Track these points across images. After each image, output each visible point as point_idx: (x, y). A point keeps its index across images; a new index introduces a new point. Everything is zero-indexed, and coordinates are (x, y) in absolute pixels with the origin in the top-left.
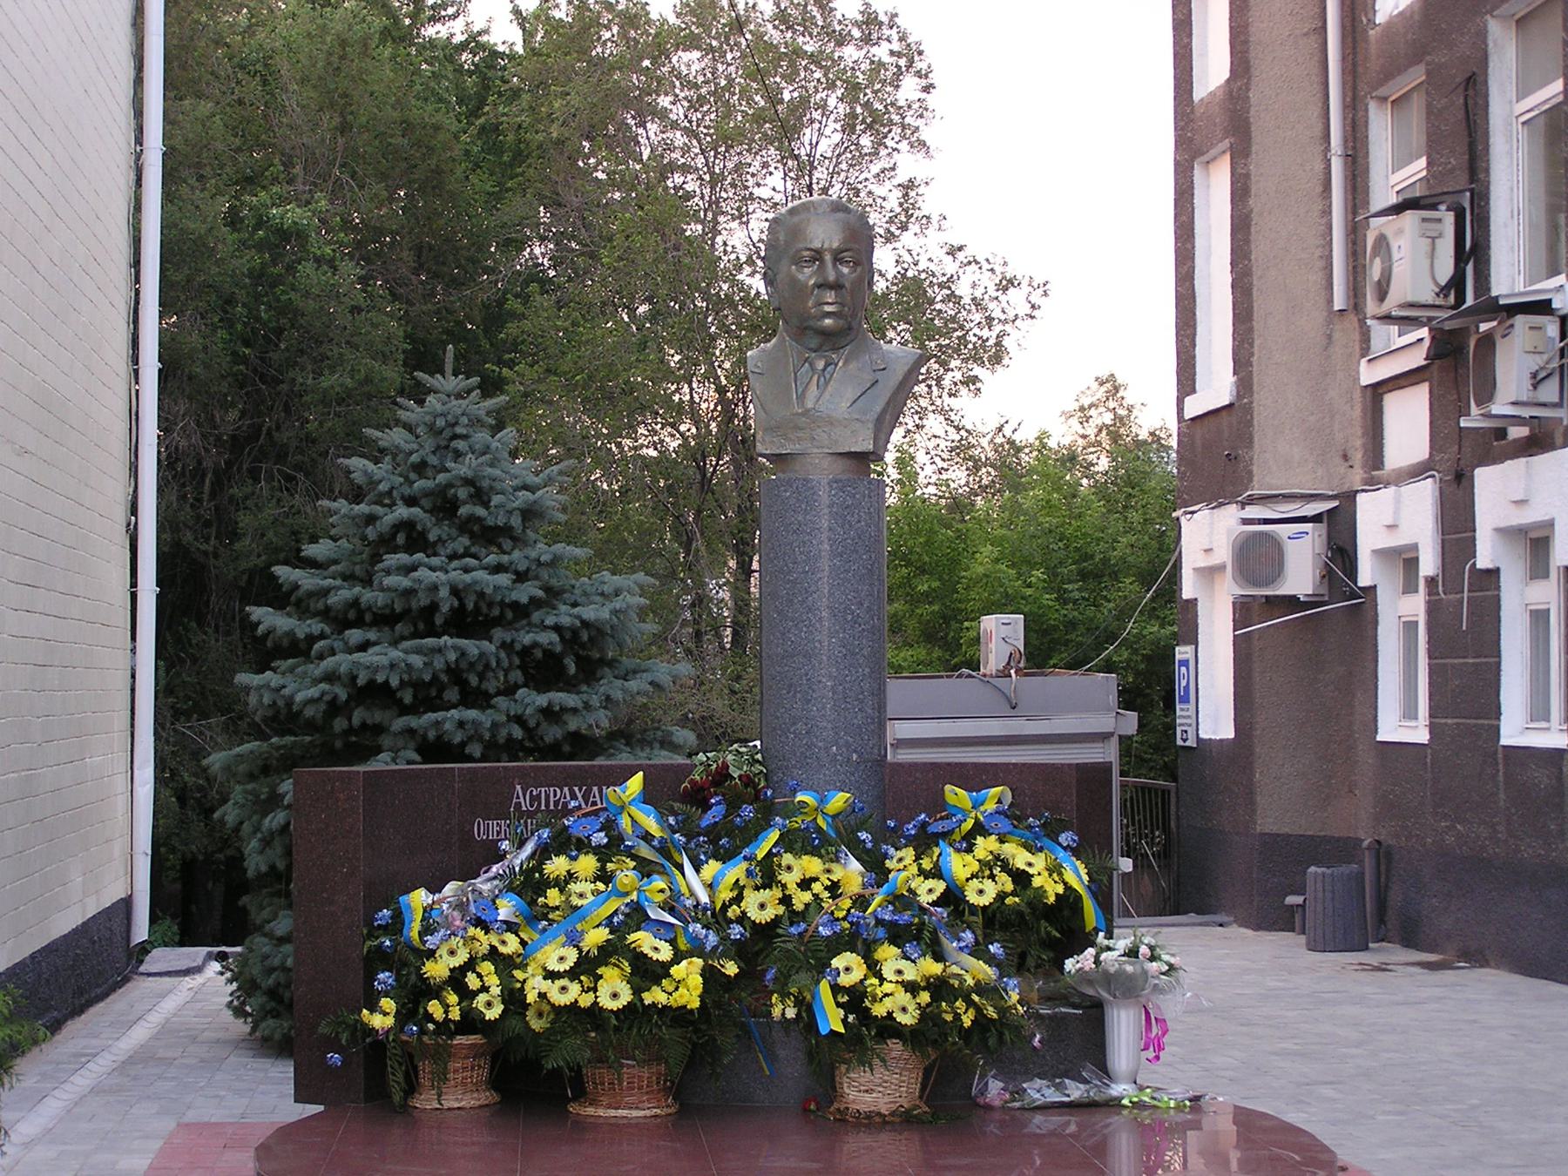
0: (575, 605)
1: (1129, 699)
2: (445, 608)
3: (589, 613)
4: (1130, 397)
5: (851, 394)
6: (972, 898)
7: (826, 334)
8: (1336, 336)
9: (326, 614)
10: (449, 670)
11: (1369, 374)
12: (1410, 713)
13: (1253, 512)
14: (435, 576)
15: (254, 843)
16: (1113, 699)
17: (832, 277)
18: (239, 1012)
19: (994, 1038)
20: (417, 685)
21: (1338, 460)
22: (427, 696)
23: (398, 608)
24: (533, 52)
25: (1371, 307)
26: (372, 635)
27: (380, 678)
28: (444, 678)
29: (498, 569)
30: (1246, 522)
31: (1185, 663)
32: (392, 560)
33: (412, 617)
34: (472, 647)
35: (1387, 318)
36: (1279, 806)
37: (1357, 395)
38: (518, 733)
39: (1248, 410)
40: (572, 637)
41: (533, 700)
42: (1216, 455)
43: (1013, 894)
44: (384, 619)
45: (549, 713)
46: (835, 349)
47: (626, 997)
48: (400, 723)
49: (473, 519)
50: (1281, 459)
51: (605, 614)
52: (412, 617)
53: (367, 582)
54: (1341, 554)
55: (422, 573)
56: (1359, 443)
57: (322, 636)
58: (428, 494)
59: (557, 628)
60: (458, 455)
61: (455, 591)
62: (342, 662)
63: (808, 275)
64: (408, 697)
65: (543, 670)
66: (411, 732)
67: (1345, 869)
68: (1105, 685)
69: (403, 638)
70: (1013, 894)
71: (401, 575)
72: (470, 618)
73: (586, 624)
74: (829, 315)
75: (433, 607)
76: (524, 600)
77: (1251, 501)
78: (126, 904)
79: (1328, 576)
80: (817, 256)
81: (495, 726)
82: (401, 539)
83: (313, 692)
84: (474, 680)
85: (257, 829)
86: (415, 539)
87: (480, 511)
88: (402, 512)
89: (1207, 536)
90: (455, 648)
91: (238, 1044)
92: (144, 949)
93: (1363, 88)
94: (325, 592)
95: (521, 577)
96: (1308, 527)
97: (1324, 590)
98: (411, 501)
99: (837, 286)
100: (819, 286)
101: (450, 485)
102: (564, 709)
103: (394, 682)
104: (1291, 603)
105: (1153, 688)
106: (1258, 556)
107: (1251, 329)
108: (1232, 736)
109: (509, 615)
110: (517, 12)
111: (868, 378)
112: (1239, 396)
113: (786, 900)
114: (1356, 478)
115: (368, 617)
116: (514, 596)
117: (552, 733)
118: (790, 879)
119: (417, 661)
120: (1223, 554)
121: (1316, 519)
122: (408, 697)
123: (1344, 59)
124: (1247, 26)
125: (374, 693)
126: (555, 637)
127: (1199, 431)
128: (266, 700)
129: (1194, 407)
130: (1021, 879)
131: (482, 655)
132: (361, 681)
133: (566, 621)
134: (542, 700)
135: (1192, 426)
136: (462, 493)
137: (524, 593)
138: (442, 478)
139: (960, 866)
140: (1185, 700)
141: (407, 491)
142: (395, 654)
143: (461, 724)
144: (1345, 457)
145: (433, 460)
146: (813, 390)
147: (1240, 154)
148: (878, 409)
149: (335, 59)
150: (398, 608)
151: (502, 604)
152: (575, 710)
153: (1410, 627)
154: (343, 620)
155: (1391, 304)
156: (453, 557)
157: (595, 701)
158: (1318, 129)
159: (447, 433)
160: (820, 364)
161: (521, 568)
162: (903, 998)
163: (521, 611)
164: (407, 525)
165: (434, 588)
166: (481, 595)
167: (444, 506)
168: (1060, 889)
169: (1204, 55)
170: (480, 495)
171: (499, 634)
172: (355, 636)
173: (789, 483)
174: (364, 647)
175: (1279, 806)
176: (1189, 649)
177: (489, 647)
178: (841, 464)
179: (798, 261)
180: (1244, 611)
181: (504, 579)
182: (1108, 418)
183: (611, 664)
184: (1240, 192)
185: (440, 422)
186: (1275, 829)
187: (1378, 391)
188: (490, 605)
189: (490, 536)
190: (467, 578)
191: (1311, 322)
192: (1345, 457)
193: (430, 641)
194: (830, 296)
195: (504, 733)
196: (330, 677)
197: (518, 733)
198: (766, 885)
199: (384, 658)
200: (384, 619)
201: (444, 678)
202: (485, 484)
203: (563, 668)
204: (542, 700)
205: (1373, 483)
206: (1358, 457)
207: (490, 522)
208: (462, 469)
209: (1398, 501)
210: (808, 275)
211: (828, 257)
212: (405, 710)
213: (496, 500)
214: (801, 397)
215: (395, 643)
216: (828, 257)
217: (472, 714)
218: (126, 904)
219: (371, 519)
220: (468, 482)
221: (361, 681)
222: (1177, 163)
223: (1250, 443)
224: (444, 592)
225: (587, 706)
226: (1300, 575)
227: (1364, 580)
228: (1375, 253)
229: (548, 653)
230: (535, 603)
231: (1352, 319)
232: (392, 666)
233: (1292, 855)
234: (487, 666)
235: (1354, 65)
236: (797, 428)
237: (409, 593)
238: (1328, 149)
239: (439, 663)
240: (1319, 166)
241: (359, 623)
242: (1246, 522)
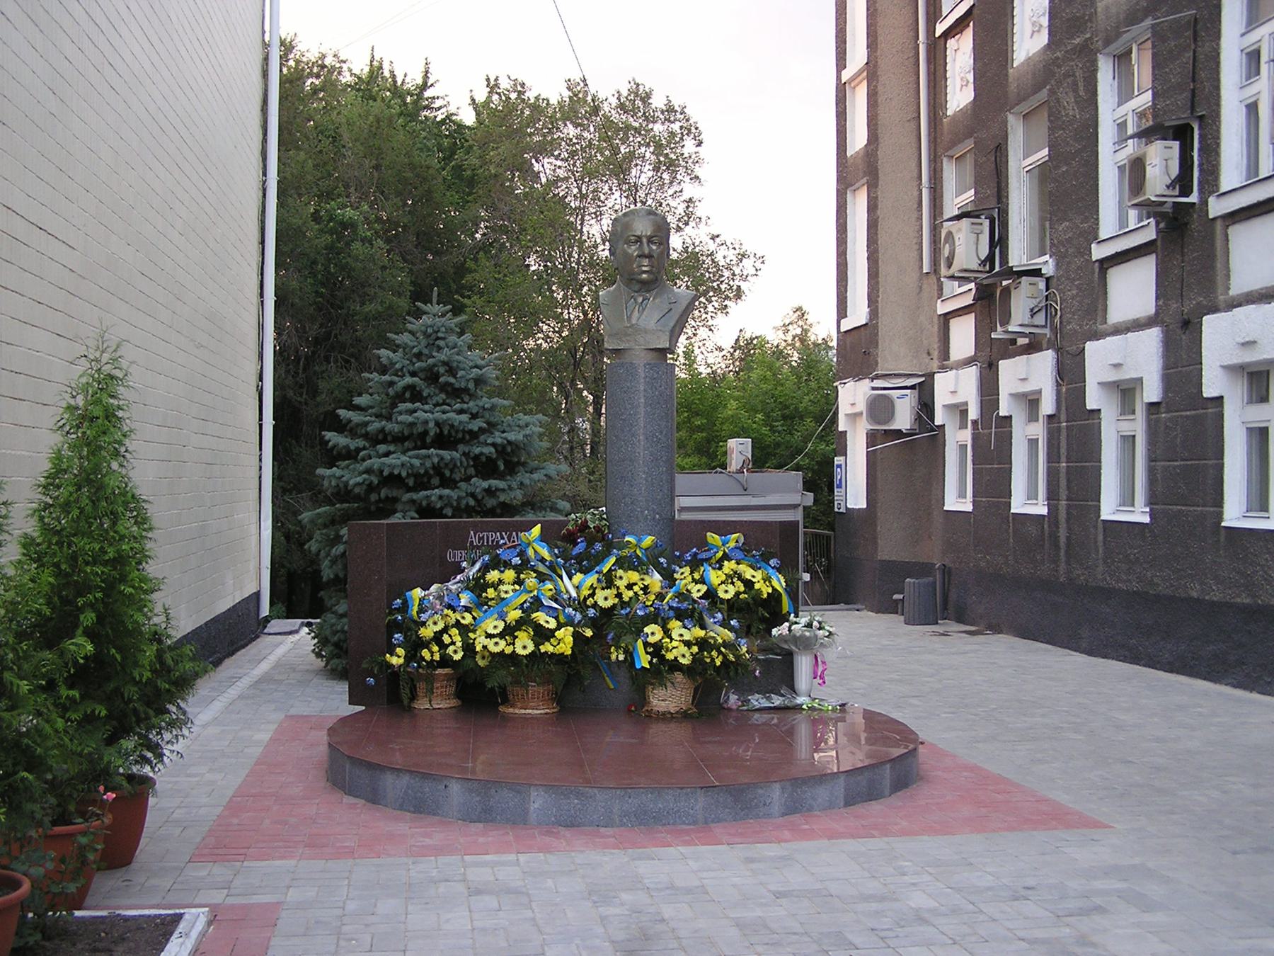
0: (504, 432)
1: (808, 486)
2: (432, 434)
3: (511, 436)
4: (811, 318)
5: (657, 316)
6: (722, 595)
7: (643, 282)
8: (925, 286)
9: (366, 436)
10: (434, 467)
11: (942, 308)
12: (962, 494)
13: (878, 383)
14: (425, 416)
15: (327, 562)
16: (800, 485)
17: (647, 251)
18: (318, 655)
19: (733, 672)
20: (416, 476)
21: (925, 355)
22: (422, 482)
23: (406, 433)
24: (480, 122)
25: (944, 271)
26: (392, 448)
27: (396, 472)
28: (431, 472)
29: (461, 412)
30: (873, 389)
31: (839, 466)
32: (403, 406)
33: (415, 439)
34: (446, 454)
35: (952, 277)
36: (891, 544)
37: (936, 320)
38: (472, 502)
39: (876, 327)
40: (501, 450)
41: (481, 484)
42: (858, 351)
43: (744, 592)
44: (399, 439)
45: (490, 492)
46: (648, 291)
47: (531, 648)
48: (407, 496)
49: (448, 384)
50: (895, 354)
51: (520, 437)
52: (415, 439)
53: (389, 418)
54: (926, 406)
55: (419, 414)
56: (936, 346)
57: (364, 448)
58: (422, 370)
59: (494, 445)
60: (439, 349)
61: (437, 424)
62: (375, 463)
63: (633, 250)
64: (411, 482)
65: (486, 468)
66: (413, 501)
67: (926, 580)
68: (796, 478)
69: (409, 450)
70: (744, 592)
71: (404, 415)
72: (445, 439)
73: (509, 442)
74: (645, 272)
75: (426, 433)
76: (476, 429)
77: (877, 377)
78: (257, 596)
79: (918, 418)
80: (639, 239)
81: (459, 498)
82: (407, 395)
83: (359, 479)
84: (447, 473)
85: (328, 555)
86: (414, 395)
87: (452, 380)
88: (408, 380)
89: (852, 397)
90: (437, 455)
91: (318, 672)
92: (267, 620)
93: (940, 151)
94: (366, 424)
95: (474, 416)
96: (908, 391)
97: (916, 427)
98: (413, 374)
99: (649, 256)
100: (639, 256)
101: (435, 365)
102: (497, 489)
103: (404, 474)
104: (898, 434)
105: (822, 480)
106: (880, 408)
107: (878, 283)
108: (865, 506)
109: (467, 437)
110: (473, 100)
111: (666, 307)
112: (871, 320)
113: (619, 595)
114: (935, 365)
115: (389, 438)
116: (470, 427)
117: (490, 503)
118: (621, 584)
119: (416, 462)
120: (861, 407)
121: (912, 387)
122: (411, 482)
123: (929, 135)
124: (877, 115)
125: (393, 480)
126: (493, 450)
127: (849, 339)
128: (333, 483)
129: (847, 325)
130: (749, 584)
131: (452, 459)
132: (385, 473)
133: (499, 441)
134: (485, 484)
135: (844, 336)
136: (442, 370)
137: (476, 425)
138: (430, 361)
139: (715, 577)
140: (840, 486)
141: (411, 368)
142: (404, 458)
143: (441, 497)
144: (929, 354)
145: (426, 351)
146: (636, 314)
147: (872, 186)
148: (672, 324)
149: (373, 129)
150: (406, 433)
151: (464, 431)
152: (503, 490)
153: (963, 448)
154: (381, 437)
155: (954, 270)
156: (436, 405)
157: (514, 485)
158: (915, 174)
159: (433, 337)
160: (640, 299)
161: (474, 411)
162: (684, 649)
163: (474, 435)
164: (411, 387)
165: (426, 422)
166: (452, 426)
167: (432, 377)
168: (770, 590)
169: (853, 131)
170: (452, 371)
171: (461, 447)
172: (382, 448)
173: (622, 365)
174: (387, 454)
175: (891, 544)
176: (842, 458)
177: (456, 455)
178: (650, 355)
179: (628, 242)
180: (872, 438)
181: (465, 417)
182: (799, 331)
183: (524, 464)
184: (872, 207)
185: (430, 330)
186: (887, 558)
187: (947, 317)
188: (457, 432)
189: (457, 393)
190: (444, 416)
191: (911, 278)
192: (929, 354)
193: (423, 452)
194: (646, 262)
195: (464, 502)
196: (368, 471)
197: (472, 502)
198: (608, 587)
199: (397, 461)
200: (399, 439)
201: (431, 472)
202: (455, 364)
203: (497, 467)
204: (485, 484)
205: (944, 368)
206: (935, 354)
207: (457, 385)
208: (442, 356)
209: (957, 378)
210: (633, 250)
211: (645, 240)
212: (409, 490)
213: (460, 373)
214: (629, 318)
215: (404, 453)
216: (645, 240)
217: (447, 492)
218: (257, 596)
219: (391, 384)
220: (445, 363)
221: (385, 473)
222: (838, 190)
223: (877, 346)
224: (431, 425)
225: (510, 488)
226: (903, 419)
227: (938, 422)
228: (946, 242)
229: (489, 458)
230: (482, 430)
231: (933, 278)
232: (403, 465)
233: (896, 572)
234: (455, 465)
235: (935, 138)
236: (626, 335)
237: (412, 425)
238: (921, 184)
239: (428, 464)
240: (916, 193)
241: (384, 441)
242: (873, 389)
